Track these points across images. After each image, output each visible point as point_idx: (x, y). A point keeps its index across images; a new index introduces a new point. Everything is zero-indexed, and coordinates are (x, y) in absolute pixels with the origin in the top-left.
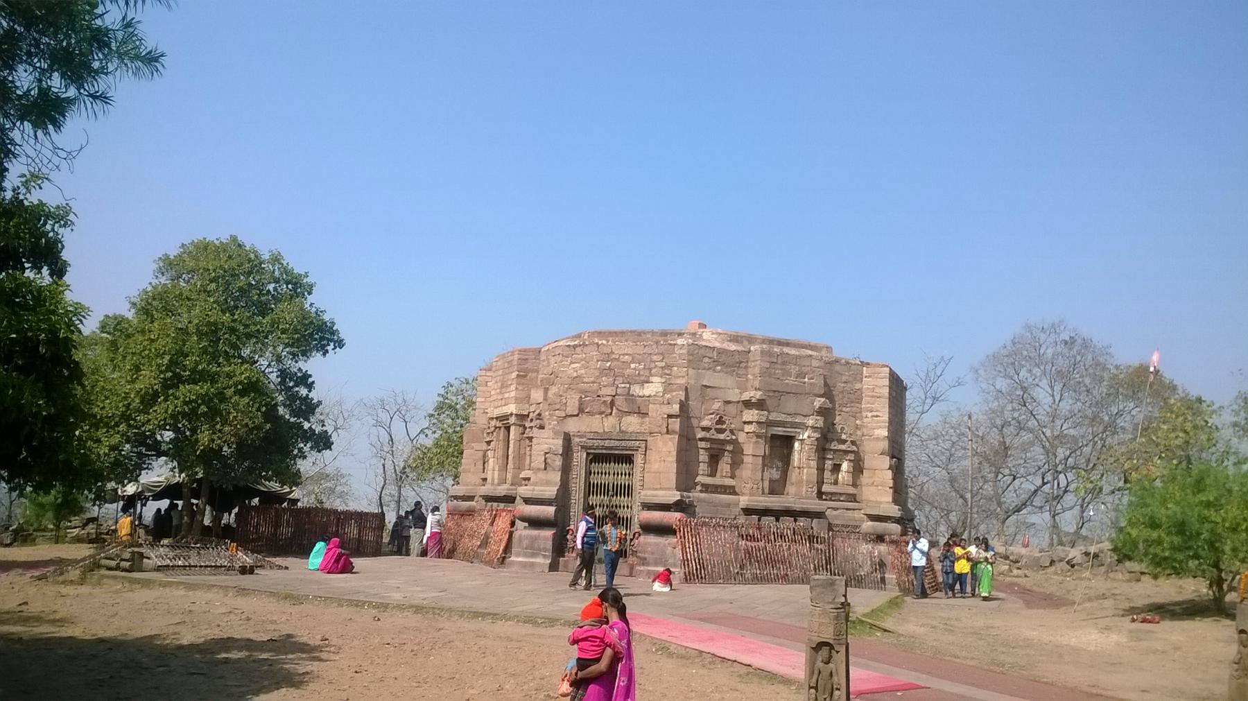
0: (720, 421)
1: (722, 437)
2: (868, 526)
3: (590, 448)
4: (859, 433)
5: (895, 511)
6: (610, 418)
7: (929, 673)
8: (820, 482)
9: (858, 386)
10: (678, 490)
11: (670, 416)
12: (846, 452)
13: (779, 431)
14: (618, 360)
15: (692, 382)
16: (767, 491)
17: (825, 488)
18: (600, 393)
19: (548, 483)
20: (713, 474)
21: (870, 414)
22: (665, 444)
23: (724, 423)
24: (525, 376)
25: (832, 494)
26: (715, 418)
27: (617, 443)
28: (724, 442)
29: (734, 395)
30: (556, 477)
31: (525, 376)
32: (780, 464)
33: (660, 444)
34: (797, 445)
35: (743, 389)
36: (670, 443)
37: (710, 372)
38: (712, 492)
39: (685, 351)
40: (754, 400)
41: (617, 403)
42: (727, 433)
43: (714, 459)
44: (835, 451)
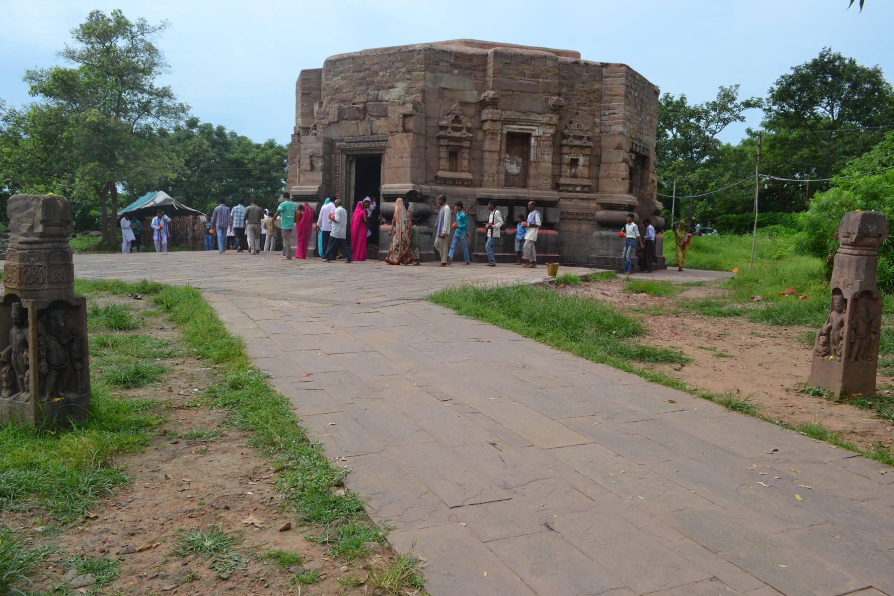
0: (457, 119)
1: (457, 134)
2: (601, 214)
3: (349, 150)
4: (597, 130)
5: (630, 199)
6: (364, 123)
7: (457, 308)
8: (556, 176)
9: (597, 86)
10: (412, 182)
11: (405, 116)
12: (582, 147)
13: (515, 128)
14: (369, 69)
15: (430, 85)
16: (503, 183)
17: (562, 181)
18: (355, 101)
19: (314, 182)
20: (453, 169)
21: (607, 113)
22: (402, 141)
23: (460, 122)
24: (307, 94)
25: (569, 185)
26: (451, 117)
27: (368, 145)
28: (460, 139)
29: (472, 96)
30: (318, 176)
31: (310, 94)
32: (520, 160)
33: (398, 141)
34: (533, 141)
35: (481, 90)
36: (406, 141)
37: (447, 76)
38: (450, 185)
39: (421, 56)
40: (487, 100)
41: (369, 109)
42: (464, 131)
43: (454, 155)
44: (572, 147)
